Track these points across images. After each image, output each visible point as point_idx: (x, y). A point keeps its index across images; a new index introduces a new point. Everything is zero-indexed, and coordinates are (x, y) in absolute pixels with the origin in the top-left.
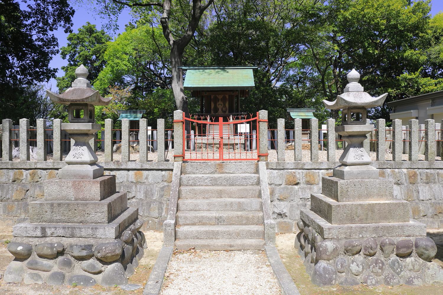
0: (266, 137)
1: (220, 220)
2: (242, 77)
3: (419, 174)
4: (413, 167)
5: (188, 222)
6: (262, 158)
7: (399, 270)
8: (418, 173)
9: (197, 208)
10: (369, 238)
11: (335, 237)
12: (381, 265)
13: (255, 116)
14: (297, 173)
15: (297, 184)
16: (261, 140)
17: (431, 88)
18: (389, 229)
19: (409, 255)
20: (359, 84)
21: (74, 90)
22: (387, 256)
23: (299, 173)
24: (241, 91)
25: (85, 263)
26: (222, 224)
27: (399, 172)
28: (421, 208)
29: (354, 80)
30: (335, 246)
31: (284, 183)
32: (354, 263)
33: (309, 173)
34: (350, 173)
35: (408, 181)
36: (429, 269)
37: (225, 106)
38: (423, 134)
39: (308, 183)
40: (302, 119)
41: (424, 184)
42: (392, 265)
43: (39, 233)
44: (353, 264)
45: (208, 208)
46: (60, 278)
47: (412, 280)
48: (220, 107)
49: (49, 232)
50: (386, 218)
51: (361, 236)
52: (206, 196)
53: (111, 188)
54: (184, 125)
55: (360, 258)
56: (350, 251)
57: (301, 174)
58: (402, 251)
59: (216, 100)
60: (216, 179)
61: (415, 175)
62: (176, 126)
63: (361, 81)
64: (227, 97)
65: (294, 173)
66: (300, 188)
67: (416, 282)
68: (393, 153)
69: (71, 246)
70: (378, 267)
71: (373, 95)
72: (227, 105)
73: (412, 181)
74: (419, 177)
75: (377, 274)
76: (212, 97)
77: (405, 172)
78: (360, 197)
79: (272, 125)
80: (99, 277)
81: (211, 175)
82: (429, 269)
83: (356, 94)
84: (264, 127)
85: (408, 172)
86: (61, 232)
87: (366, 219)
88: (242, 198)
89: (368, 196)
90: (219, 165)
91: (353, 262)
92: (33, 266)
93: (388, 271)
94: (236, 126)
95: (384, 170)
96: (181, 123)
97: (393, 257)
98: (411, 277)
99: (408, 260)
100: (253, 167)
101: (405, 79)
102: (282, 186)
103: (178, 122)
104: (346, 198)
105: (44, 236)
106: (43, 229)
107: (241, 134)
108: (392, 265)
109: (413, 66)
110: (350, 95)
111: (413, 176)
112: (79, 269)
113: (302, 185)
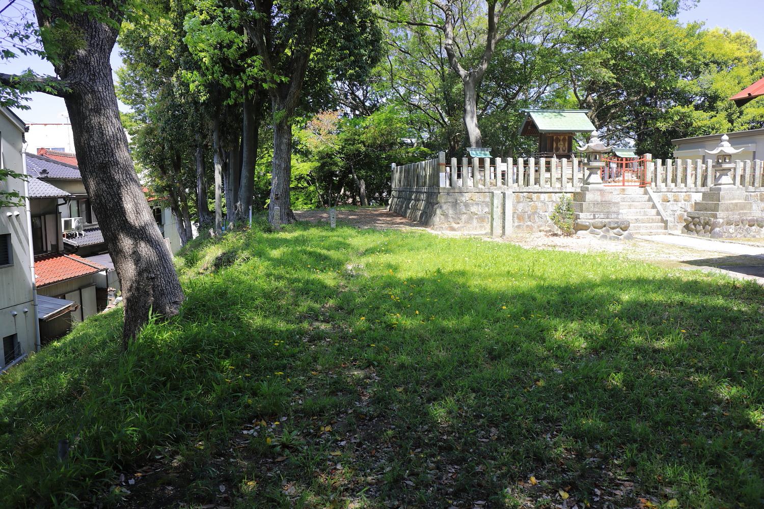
10: (737, 217)
15: (669, 201)
17: (705, 122)
18: (745, 214)
19: (753, 225)
22: (744, 226)
25: (615, 231)
29: (725, 140)
34: (724, 189)
38: (515, 177)
39: (675, 201)
42: (746, 230)
43: (592, 217)
46: (604, 237)
49: (597, 216)
50: (742, 209)
55: (733, 226)
56: (729, 223)
58: (751, 223)
59: (558, 140)
63: (728, 141)
68: (696, 186)
69: (610, 222)
75: (741, 234)
78: (730, 200)
80: (621, 237)
86: (602, 216)
89: (734, 199)
92: (592, 233)
93: (745, 233)
97: (747, 226)
99: (753, 227)
101: (677, 113)
105: (594, 218)
106: (594, 215)
108: (746, 230)
109: (683, 98)
112: (612, 233)
113: (671, 202)
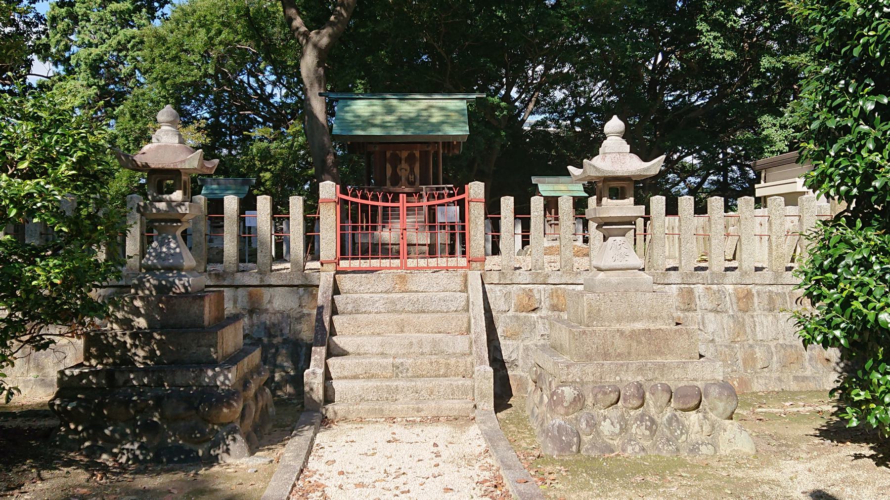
0: (482, 228)
1: (401, 368)
2: (444, 113)
3: (756, 294)
4: (744, 282)
5: (346, 374)
6: (474, 264)
7: (679, 432)
8: (754, 291)
9: (362, 351)
11: (578, 380)
12: (648, 423)
13: (462, 191)
14: (535, 292)
16: (472, 233)
20: (624, 141)
21: (159, 147)
23: (539, 291)
24: (444, 143)
26: (404, 375)
27: (719, 291)
28: (758, 355)
30: (576, 392)
31: (512, 309)
32: (607, 420)
33: (557, 291)
35: (735, 307)
36: (725, 430)
37: (412, 171)
40: (574, 197)
41: (766, 313)
44: (604, 421)
45: (380, 350)
47: (698, 448)
48: (403, 174)
51: (618, 378)
52: (377, 331)
53: (218, 310)
54: (338, 207)
57: (543, 292)
59: (396, 161)
60: (393, 302)
61: (749, 295)
62: (322, 207)
64: (417, 155)
65: (531, 290)
66: (541, 317)
67: (703, 449)
70: (644, 427)
71: (645, 159)
72: (417, 170)
73: (742, 306)
74: (756, 300)
76: (388, 155)
77: (731, 291)
79: (522, 212)
81: (386, 296)
82: (725, 430)
83: (615, 156)
84: (477, 212)
85: (735, 290)
87: (629, 353)
88: (440, 332)
89: (635, 318)
90: (400, 277)
91: (605, 418)
94: (432, 210)
95: (692, 286)
96: (333, 205)
98: (697, 443)
100: (459, 280)
102: (510, 314)
103: (328, 201)
104: (598, 321)
107: (443, 227)
110: (606, 159)
111: (744, 297)
113: (544, 312)
